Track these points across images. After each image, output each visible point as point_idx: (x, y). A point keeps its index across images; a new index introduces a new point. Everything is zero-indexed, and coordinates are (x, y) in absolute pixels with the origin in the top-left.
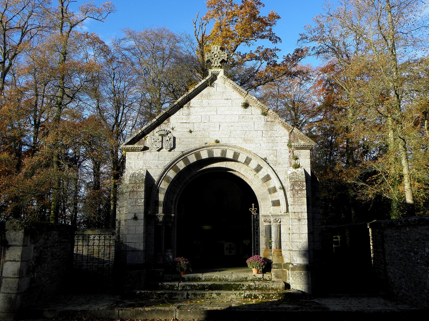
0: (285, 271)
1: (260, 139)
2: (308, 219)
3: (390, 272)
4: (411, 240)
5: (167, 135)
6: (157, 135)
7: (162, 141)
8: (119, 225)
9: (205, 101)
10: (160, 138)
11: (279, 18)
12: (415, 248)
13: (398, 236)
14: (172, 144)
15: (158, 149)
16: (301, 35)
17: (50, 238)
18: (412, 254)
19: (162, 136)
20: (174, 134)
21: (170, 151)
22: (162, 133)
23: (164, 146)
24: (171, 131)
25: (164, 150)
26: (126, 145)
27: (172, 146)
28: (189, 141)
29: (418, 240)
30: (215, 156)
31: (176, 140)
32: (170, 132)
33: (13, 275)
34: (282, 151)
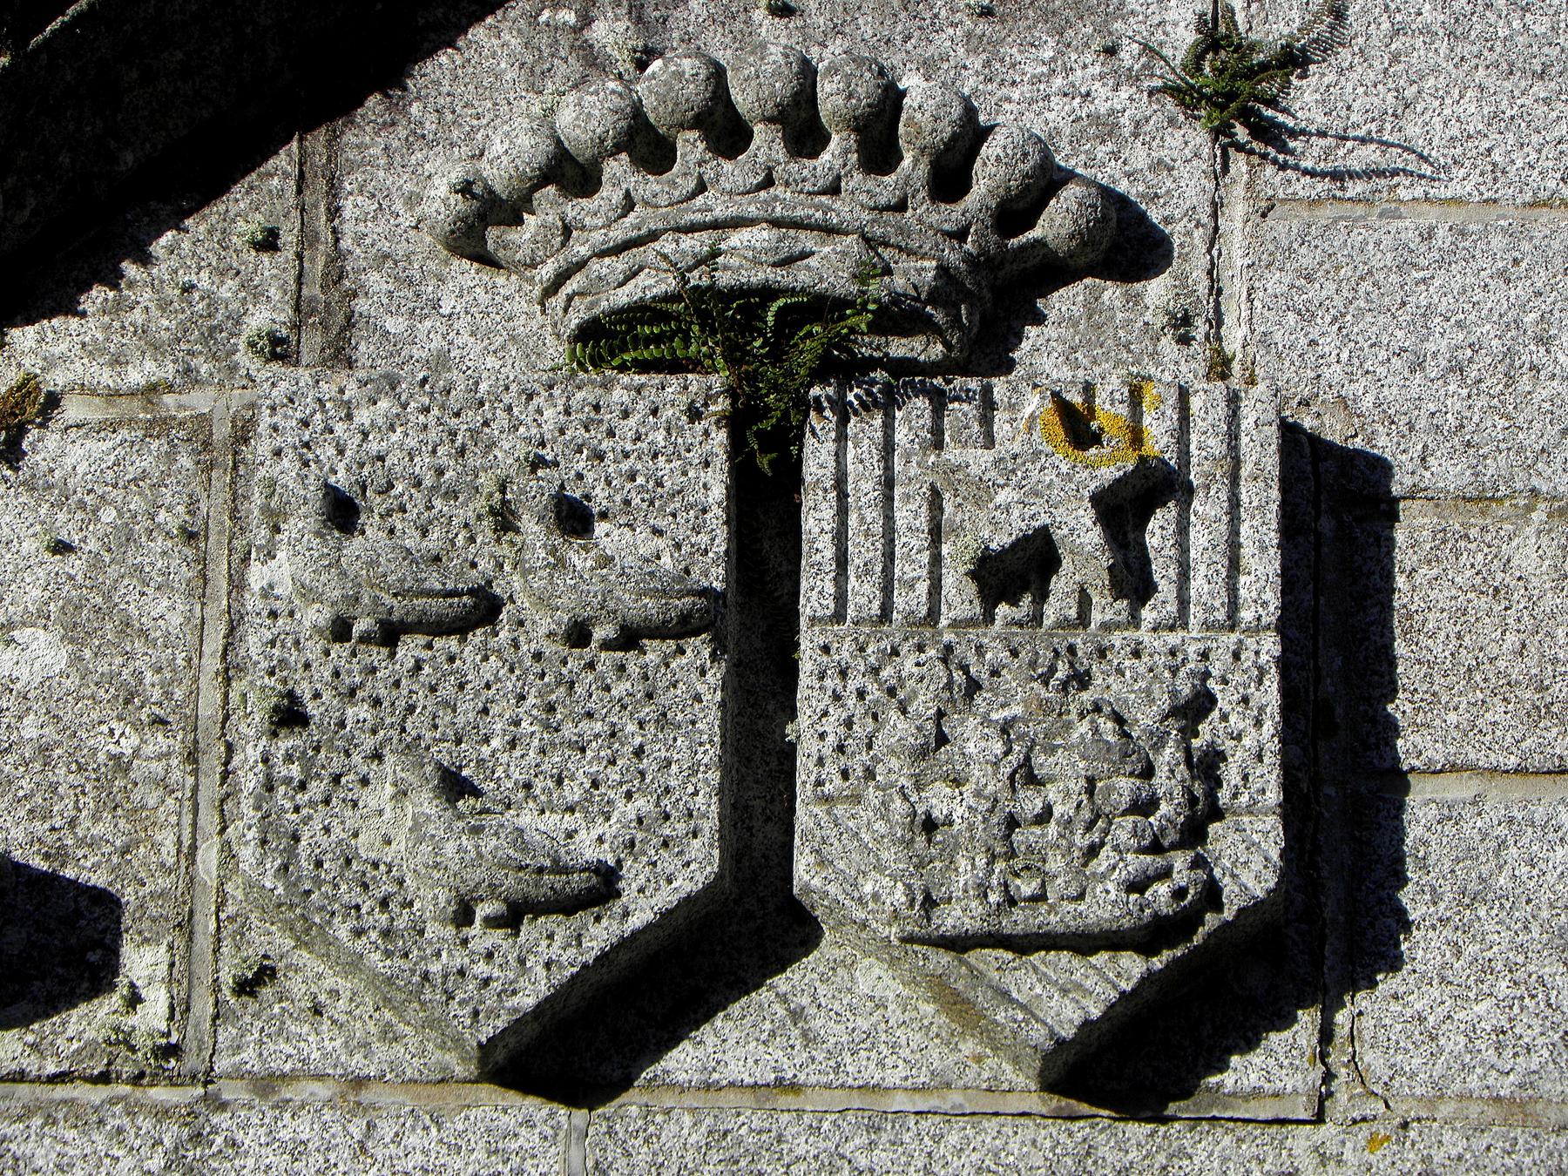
2: (1395, 782)
5: (989, 349)
6: (495, 329)
7: (752, 618)
10: (667, 455)
14: (1250, 733)
15: (551, 957)
19: (770, 364)
20: (1292, 314)
21: (1132, 1066)
22: (752, 225)
23: (840, 854)
24: (1168, 166)
25: (847, 1007)
27: (1249, 858)
31: (1427, 580)
32: (1127, 244)
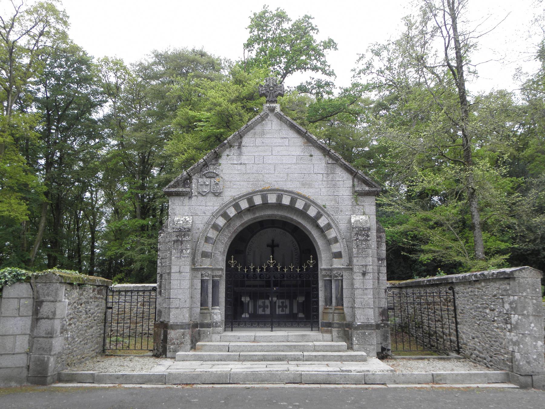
0: (348, 331)
1: (320, 183)
3: (463, 333)
4: (486, 296)
8: (161, 279)
9: (258, 141)
11: (336, 49)
12: (491, 304)
13: (471, 292)
16: (352, 70)
17: (84, 293)
18: (488, 311)
26: (169, 188)
28: (240, 185)
29: (495, 296)
30: (269, 202)
33: (46, 334)
34: (345, 197)
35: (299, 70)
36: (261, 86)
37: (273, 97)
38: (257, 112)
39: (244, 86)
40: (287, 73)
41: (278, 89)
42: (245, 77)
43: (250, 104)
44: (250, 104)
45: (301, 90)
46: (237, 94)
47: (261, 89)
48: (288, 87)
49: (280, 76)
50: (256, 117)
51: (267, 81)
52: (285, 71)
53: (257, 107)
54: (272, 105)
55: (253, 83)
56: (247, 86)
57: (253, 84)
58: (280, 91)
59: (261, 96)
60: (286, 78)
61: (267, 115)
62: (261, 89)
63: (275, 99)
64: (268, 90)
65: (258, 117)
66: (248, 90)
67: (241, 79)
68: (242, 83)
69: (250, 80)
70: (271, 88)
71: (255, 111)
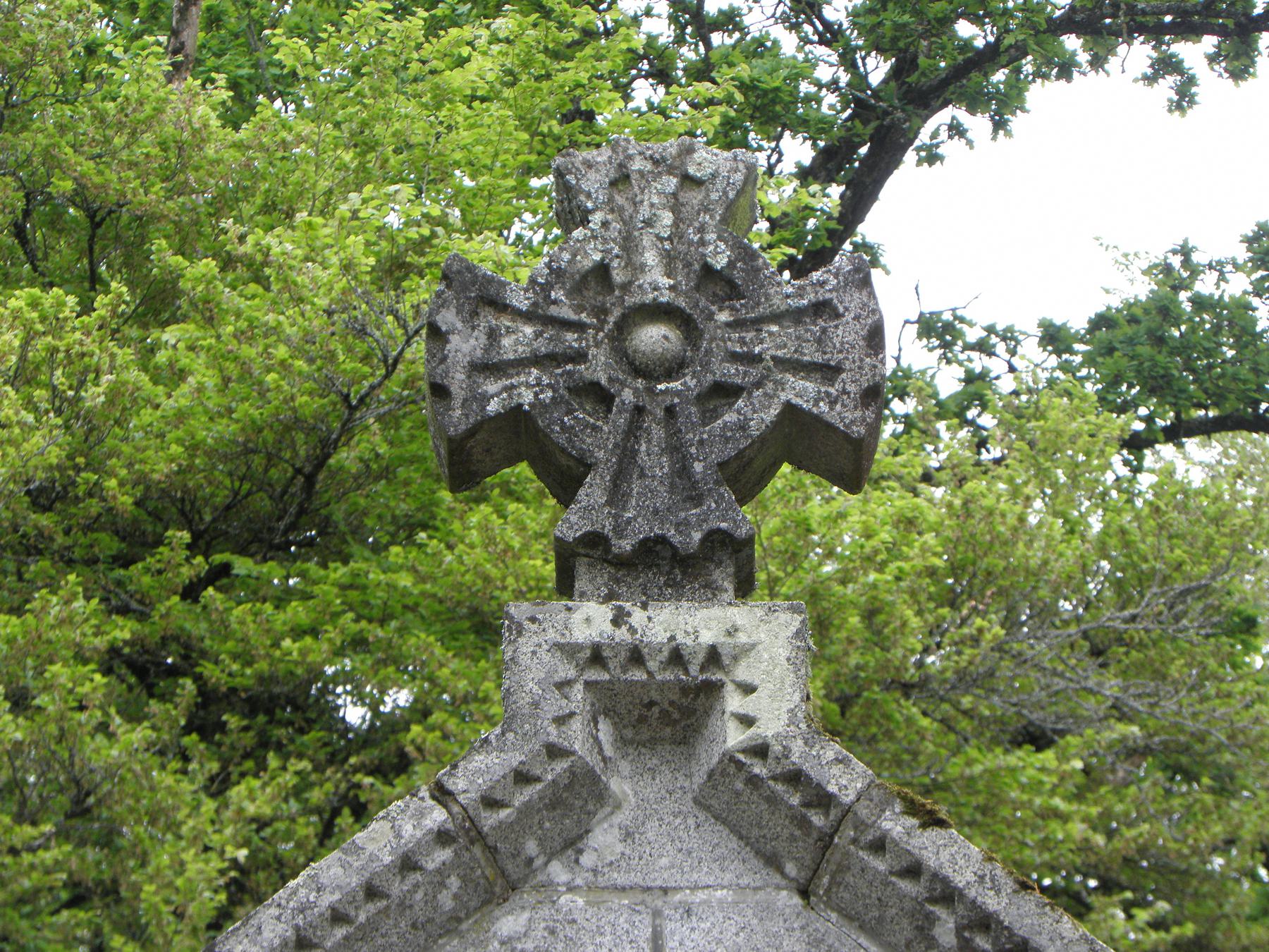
35: (1136, 55)
36: (478, 294)
37: (688, 490)
38: (390, 755)
39: (159, 303)
40: (918, 91)
41: (774, 341)
42: (181, 155)
43: (263, 622)
44: (263, 622)
45: (1158, 386)
46: (45, 446)
47: (465, 345)
48: (940, 330)
49: (798, 150)
50: (377, 841)
51: (570, 214)
52: (877, 69)
53: (393, 661)
54: (671, 622)
55: (321, 257)
56: (209, 315)
57: (322, 280)
58: (801, 391)
59: (467, 465)
60: (906, 182)
61: (573, 802)
62: (465, 345)
63: (720, 511)
64: (599, 367)
65: (403, 822)
66: (237, 377)
67: (113, 181)
68: (134, 259)
69: (278, 211)
70: (654, 337)
71: (342, 747)
